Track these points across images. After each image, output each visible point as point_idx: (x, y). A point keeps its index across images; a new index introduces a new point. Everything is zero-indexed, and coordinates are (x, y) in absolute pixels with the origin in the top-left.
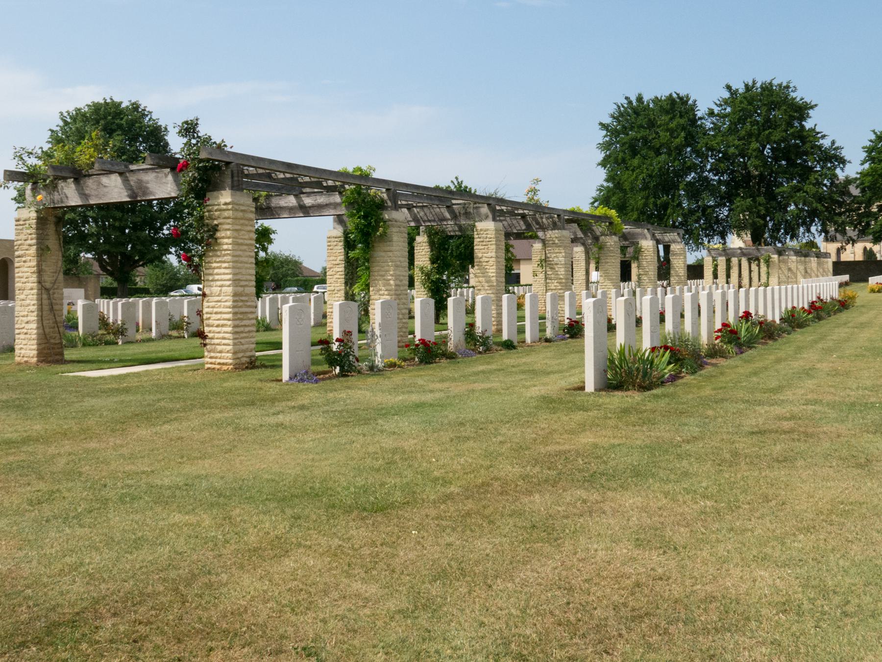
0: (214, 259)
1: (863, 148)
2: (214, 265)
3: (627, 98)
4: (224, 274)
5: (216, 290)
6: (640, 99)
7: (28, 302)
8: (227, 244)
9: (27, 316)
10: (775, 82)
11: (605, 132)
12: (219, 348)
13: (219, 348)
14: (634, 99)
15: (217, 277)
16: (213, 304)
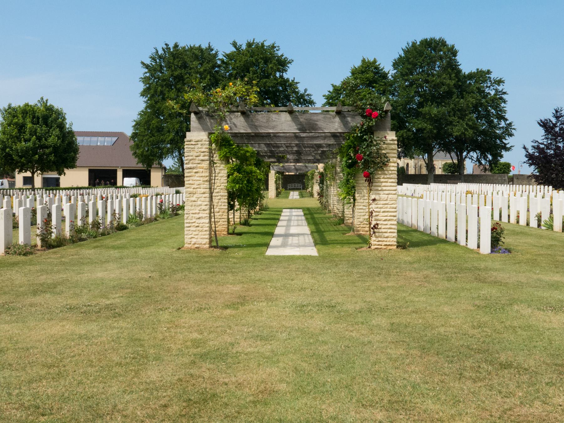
0: (382, 176)
1: (324, 96)
2: (382, 180)
3: (166, 44)
4: (391, 186)
5: (383, 196)
6: (176, 46)
7: (199, 203)
8: (393, 166)
9: (199, 213)
10: (266, 44)
11: (147, 70)
12: (386, 235)
13: (386, 235)
14: (171, 46)
15: (384, 188)
16: (381, 206)
